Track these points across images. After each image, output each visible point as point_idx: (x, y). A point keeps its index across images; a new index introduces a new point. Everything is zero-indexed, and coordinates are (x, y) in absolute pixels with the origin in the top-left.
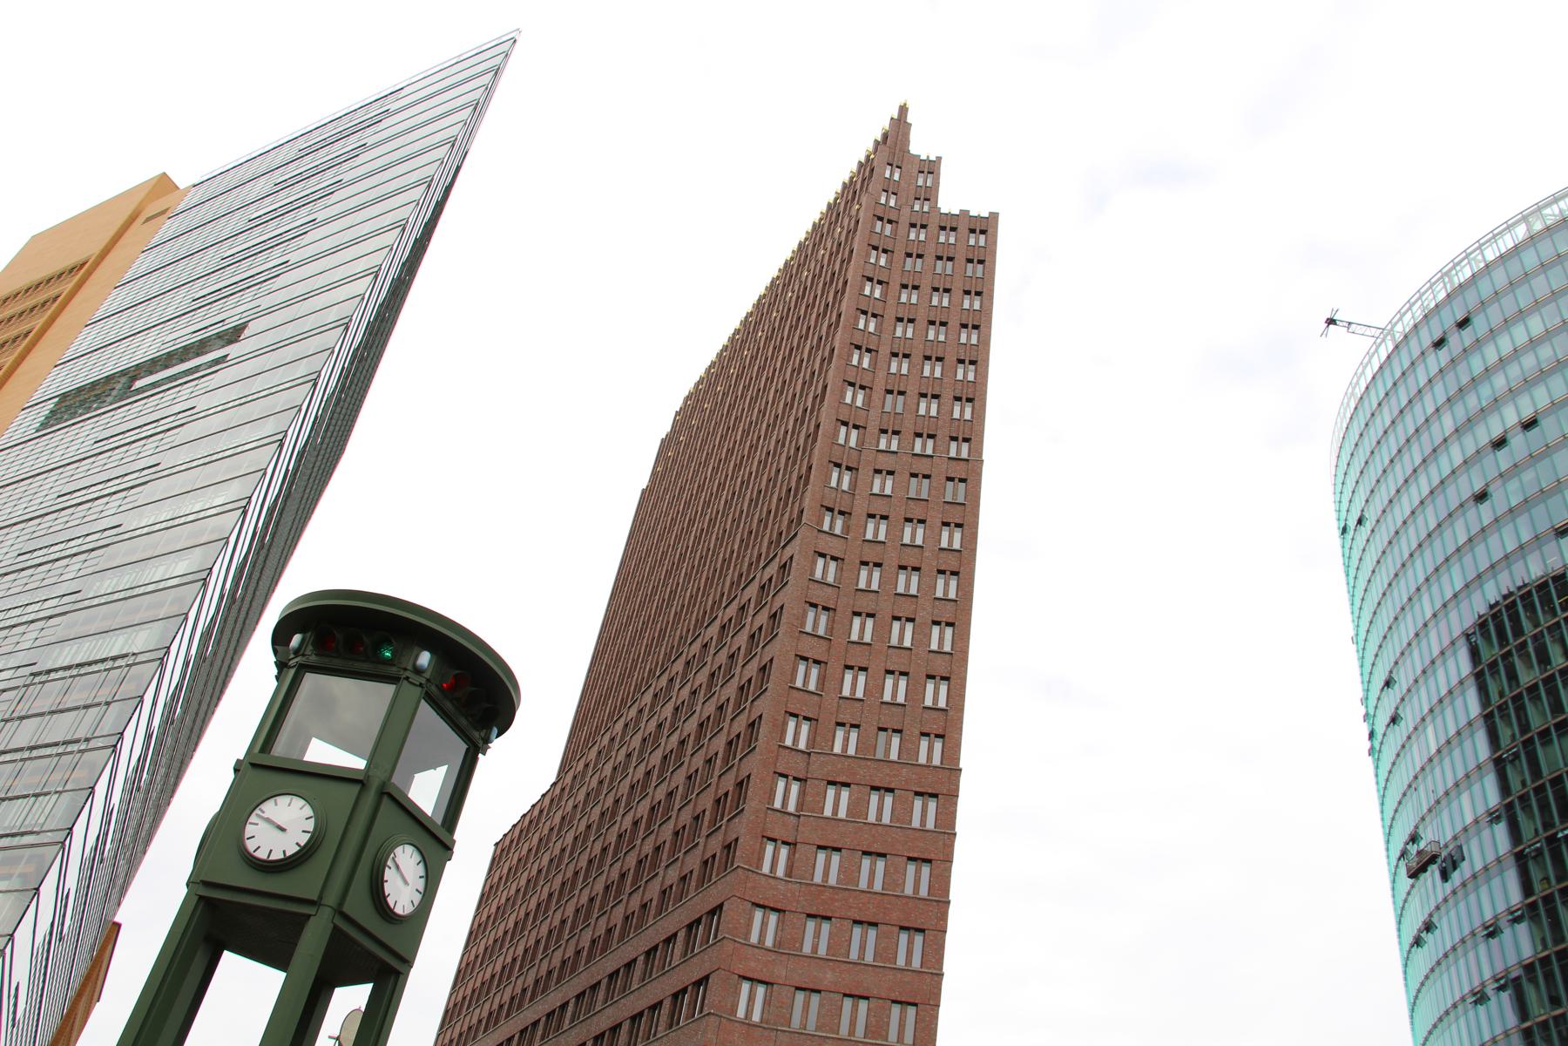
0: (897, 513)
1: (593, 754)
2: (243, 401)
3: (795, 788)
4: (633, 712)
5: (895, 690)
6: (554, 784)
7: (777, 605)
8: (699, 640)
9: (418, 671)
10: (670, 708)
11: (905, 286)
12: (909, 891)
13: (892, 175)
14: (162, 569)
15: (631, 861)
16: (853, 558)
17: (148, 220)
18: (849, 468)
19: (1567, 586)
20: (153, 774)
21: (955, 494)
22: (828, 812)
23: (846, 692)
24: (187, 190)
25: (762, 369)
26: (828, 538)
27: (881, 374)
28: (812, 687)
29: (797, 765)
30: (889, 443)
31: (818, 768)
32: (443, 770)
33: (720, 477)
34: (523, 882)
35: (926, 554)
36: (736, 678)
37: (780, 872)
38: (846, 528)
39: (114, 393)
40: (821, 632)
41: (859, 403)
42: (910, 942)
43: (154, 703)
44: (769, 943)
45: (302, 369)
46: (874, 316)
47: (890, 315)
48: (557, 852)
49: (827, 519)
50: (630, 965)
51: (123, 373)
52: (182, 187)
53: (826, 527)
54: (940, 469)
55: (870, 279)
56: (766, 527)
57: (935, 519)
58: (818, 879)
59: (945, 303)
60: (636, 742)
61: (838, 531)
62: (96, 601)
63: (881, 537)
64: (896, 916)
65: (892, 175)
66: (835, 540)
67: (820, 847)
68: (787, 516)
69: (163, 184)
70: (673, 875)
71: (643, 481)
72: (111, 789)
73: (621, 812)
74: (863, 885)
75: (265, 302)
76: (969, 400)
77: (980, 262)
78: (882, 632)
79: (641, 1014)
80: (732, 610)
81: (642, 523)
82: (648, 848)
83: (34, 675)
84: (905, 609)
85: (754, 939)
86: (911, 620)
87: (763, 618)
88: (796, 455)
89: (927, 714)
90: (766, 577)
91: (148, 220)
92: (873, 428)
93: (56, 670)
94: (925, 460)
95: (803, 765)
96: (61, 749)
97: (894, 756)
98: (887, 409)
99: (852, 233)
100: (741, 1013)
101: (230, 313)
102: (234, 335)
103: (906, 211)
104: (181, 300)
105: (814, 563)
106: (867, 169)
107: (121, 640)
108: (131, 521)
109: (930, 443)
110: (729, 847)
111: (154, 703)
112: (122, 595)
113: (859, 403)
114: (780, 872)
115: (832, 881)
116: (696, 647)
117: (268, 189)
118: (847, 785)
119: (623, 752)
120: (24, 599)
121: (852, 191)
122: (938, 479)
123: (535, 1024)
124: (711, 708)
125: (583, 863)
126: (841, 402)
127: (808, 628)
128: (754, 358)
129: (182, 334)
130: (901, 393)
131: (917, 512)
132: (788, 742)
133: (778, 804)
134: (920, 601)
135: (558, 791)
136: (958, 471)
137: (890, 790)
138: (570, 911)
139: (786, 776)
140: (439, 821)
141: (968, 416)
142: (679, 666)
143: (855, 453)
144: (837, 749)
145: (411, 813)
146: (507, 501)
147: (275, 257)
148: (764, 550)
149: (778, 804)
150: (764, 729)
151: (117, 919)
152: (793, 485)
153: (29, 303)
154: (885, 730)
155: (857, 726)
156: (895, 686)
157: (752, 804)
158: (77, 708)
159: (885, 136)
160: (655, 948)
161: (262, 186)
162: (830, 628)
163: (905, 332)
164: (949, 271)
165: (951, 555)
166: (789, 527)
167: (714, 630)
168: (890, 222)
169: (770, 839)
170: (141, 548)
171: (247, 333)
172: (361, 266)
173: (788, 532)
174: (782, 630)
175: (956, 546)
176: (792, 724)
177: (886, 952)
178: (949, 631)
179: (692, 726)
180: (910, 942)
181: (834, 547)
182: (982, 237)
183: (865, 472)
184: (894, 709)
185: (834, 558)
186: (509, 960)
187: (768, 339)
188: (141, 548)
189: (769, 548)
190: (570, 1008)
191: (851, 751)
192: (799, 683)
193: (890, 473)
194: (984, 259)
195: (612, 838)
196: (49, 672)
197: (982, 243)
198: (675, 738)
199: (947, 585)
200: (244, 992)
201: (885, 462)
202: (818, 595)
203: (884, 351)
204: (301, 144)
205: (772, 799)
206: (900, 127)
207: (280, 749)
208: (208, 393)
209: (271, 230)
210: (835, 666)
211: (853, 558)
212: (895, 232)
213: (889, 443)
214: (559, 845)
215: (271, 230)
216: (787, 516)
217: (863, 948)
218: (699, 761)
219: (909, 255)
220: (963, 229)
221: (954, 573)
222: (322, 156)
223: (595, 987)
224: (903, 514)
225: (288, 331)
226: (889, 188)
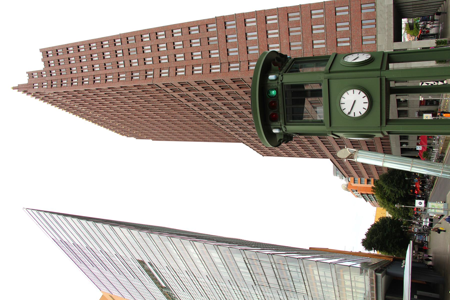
0: (142, 56)
1: (232, 133)
5: (196, 43)
6: (243, 143)
7: (179, 85)
11: (71, 73)
12: (255, 24)
16: (159, 66)
18: (132, 74)
21: (132, 40)
22: (237, 54)
24: (102, 292)
25: (108, 112)
26: (155, 75)
27: (101, 72)
28: (201, 68)
29: (225, 66)
30: (121, 64)
31: (224, 60)
33: (143, 116)
35: (153, 44)
36: (203, 92)
39: (168, 291)
40: (184, 69)
46: (83, 79)
47: (81, 75)
51: (162, 291)
52: (102, 294)
54: (125, 46)
55: (72, 84)
57: (141, 44)
59: (73, 59)
61: (152, 72)
63: (151, 59)
64: (263, 26)
66: (155, 73)
67: (248, 53)
68: (151, 90)
74: (256, 38)
75: (130, 257)
76: (102, 43)
77: (57, 51)
78: (179, 51)
81: (162, 138)
84: (171, 46)
86: (174, 43)
87: (183, 88)
89: (201, 31)
90: (171, 91)
92: (118, 70)
94: (124, 52)
95: (225, 64)
97: (216, 38)
98: (111, 68)
99: (59, 94)
101: (136, 266)
102: (142, 263)
103: (47, 79)
104: (136, 282)
105: (163, 77)
106: (37, 95)
109: (118, 52)
115: (257, 47)
117: (95, 268)
118: (228, 50)
122: (129, 46)
127: (183, 73)
129: (146, 278)
130: (105, 65)
131: (140, 50)
132: (219, 70)
134: (167, 42)
135: (245, 141)
136: (125, 41)
139: (229, 68)
141: (107, 42)
143: (127, 74)
144: (218, 56)
147: (115, 259)
149: (238, 69)
150: (217, 78)
151: (309, 249)
154: (209, 43)
155: (209, 51)
156: (195, 43)
157: (239, 76)
159: (25, 92)
161: (95, 270)
162: (182, 67)
163: (86, 69)
164: (63, 60)
165: (151, 36)
166: (154, 88)
167: (189, 104)
168: (52, 83)
169: (249, 68)
171: (140, 259)
174: (186, 81)
175: (148, 35)
177: (274, 27)
178: (174, 31)
181: (157, 72)
182: (49, 52)
183: (132, 69)
184: (202, 42)
185: (161, 71)
187: (98, 112)
191: (217, 51)
194: (56, 50)
197: (51, 52)
198: (224, 107)
199: (161, 35)
201: (128, 64)
202: (173, 73)
203: (93, 73)
204: (79, 263)
206: (21, 88)
208: (161, 264)
210: (193, 63)
211: (159, 66)
212: (55, 80)
217: (274, 34)
219: (61, 74)
220: (48, 59)
221: (157, 34)
222: (80, 255)
224: (142, 54)
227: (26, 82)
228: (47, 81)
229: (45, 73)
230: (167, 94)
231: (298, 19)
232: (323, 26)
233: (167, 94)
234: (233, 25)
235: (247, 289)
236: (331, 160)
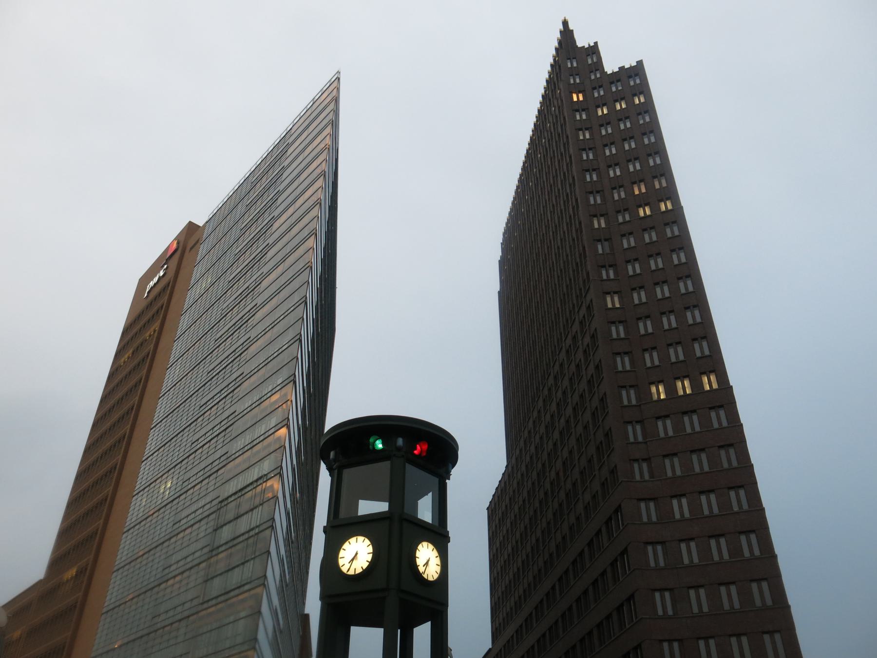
2: (273, 325)
3: (652, 505)
4: (535, 414)
7: (593, 330)
8: (557, 363)
9: (399, 449)
10: (554, 405)
13: (573, 62)
14: (264, 426)
15: (562, 495)
17: (191, 249)
19: (447, 655)
20: (296, 531)
22: (662, 435)
23: (649, 364)
28: (628, 368)
30: (624, 217)
32: (430, 494)
34: (509, 525)
36: (584, 377)
37: (647, 477)
38: (616, 273)
41: (599, 201)
42: (737, 495)
43: (284, 497)
44: (654, 519)
45: (296, 298)
48: (521, 503)
49: (604, 273)
50: (581, 554)
52: (201, 225)
53: (605, 277)
56: (571, 289)
58: (670, 474)
60: (542, 430)
62: (237, 454)
65: (573, 62)
68: (581, 279)
69: (191, 227)
70: (588, 497)
71: (496, 286)
72: (277, 548)
73: (548, 470)
78: (657, 324)
79: (596, 580)
80: (569, 341)
82: (569, 486)
83: (221, 502)
85: (645, 519)
87: (587, 340)
88: (574, 243)
91: (191, 249)
93: (231, 496)
96: (246, 536)
100: (652, 564)
106: (556, 67)
107: (256, 470)
108: (239, 407)
110: (613, 472)
111: (284, 497)
112: (249, 447)
113: (599, 201)
114: (647, 477)
116: (557, 367)
119: (538, 437)
120: (193, 508)
121: (552, 84)
123: (541, 601)
124: (576, 398)
125: (537, 505)
126: (589, 205)
128: (532, 199)
133: (632, 439)
137: (694, 411)
138: (539, 533)
140: (437, 524)
142: (551, 381)
145: (422, 524)
146: (422, 328)
148: (575, 302)
149: (632, 439)
151: (306, 612)
152: (578, 260)
153: (150, 314)
158: (247, 513)
160: (592, 540)
167: (563, 354)
170: (248, 419)
172: (306, 232)
173: (585, 288)
176: (624, 393)
179: (569, 411)
180: (737, 495)
186: (516, 570)
188: (248, 419)
189: (577, 300)
190: (557, 587)
192: (620, 368)
193: (631, 233)
194: (644, 89)
195: (548, 486)
196: (227, 498)
198: (562, 420)
200: (366, 646)
205: (628, 438)
206: (567, 34)
207: (343, 514)
209: (260, 205)
213: (624, 217)
214: (521, 498)
215: (260, 205)
216: (581, 279)
218: (580, 429)
223: (566, 572)
225: (283, 280)
226: (573, 72)
227: (579, 44)
228: (582, 83)
229: (598, 76)
230: (576, 310)
231: (747, 554)
232: (737, 605)
233: (576, 310)
234: (720, 423)
235: (212, 488)
236: (490, 650)
